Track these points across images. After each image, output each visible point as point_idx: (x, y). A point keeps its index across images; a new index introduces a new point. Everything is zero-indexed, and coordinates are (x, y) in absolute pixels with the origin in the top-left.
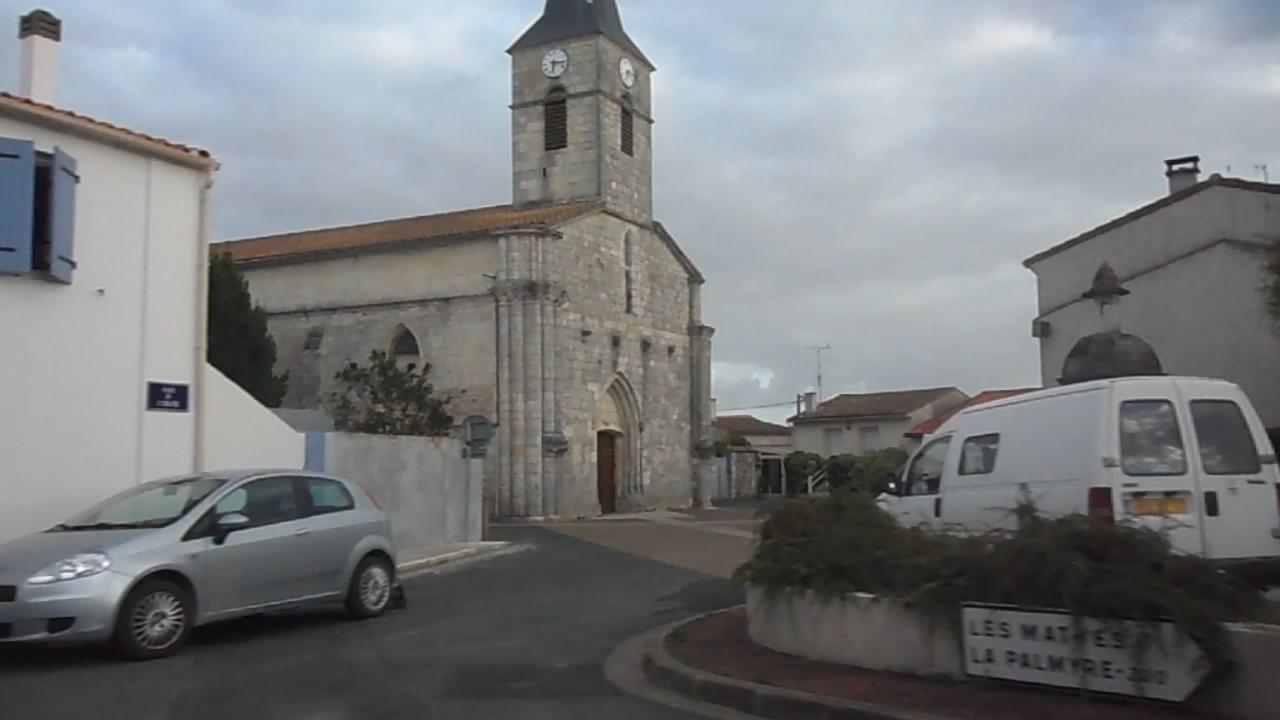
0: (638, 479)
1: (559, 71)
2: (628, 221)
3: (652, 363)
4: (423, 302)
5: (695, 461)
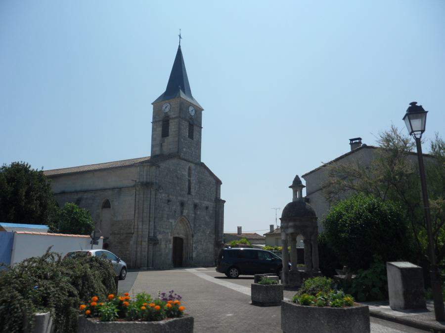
0: (191, 255)
1: (167, 110)
2: (189, 162)
3: (199, 213)
4: (113, 189)
5: (216, 249)
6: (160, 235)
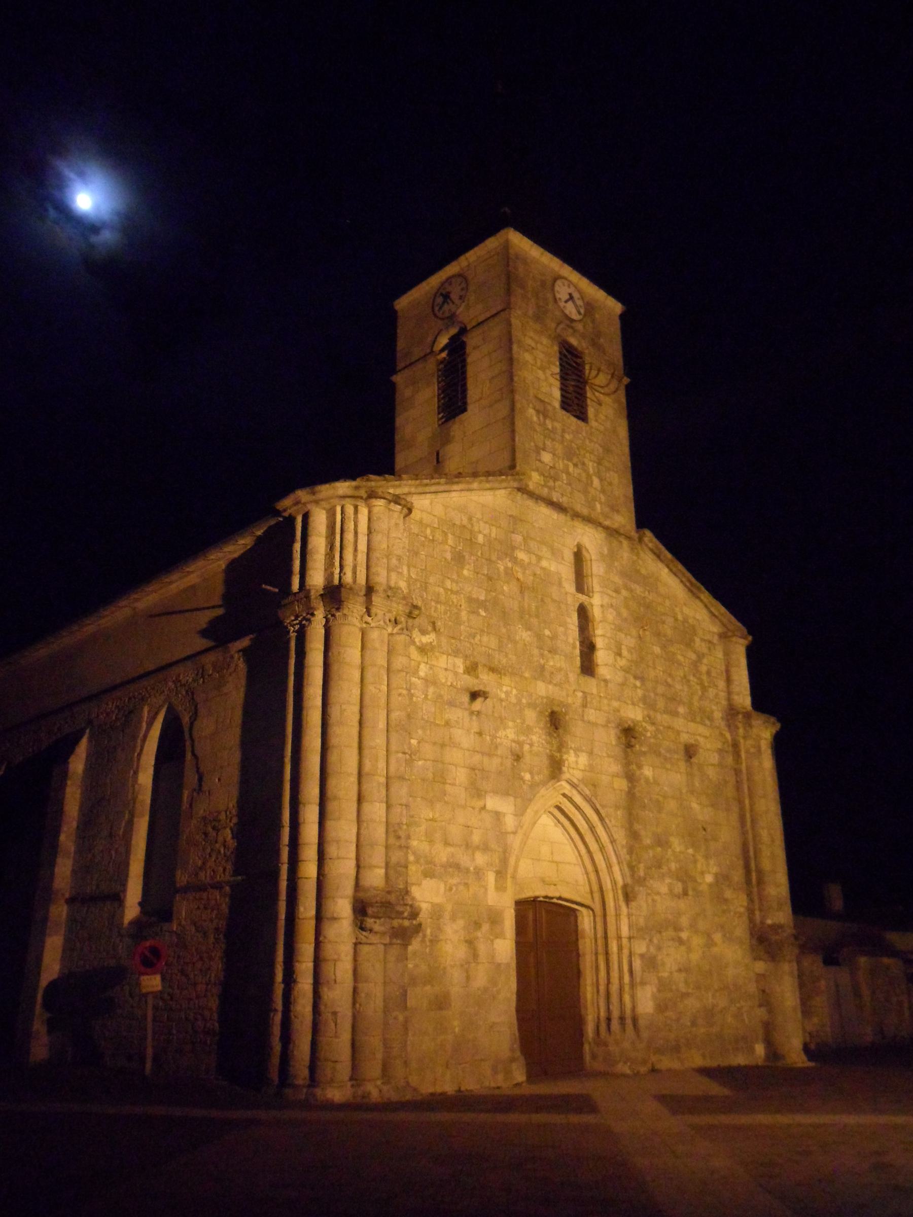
0: (627, 998)
3: (648, 772)
5: (760, 967)
6: (428, 883)
